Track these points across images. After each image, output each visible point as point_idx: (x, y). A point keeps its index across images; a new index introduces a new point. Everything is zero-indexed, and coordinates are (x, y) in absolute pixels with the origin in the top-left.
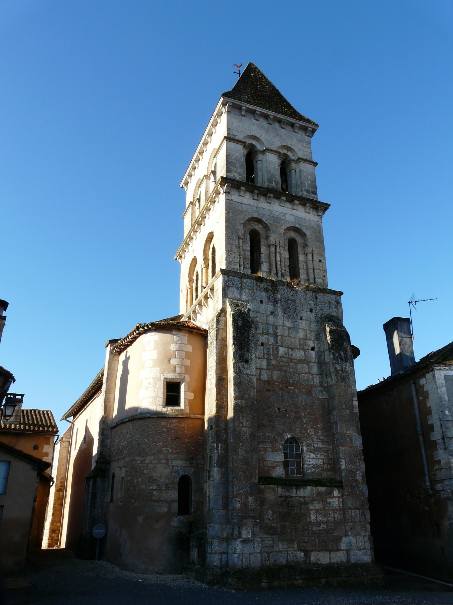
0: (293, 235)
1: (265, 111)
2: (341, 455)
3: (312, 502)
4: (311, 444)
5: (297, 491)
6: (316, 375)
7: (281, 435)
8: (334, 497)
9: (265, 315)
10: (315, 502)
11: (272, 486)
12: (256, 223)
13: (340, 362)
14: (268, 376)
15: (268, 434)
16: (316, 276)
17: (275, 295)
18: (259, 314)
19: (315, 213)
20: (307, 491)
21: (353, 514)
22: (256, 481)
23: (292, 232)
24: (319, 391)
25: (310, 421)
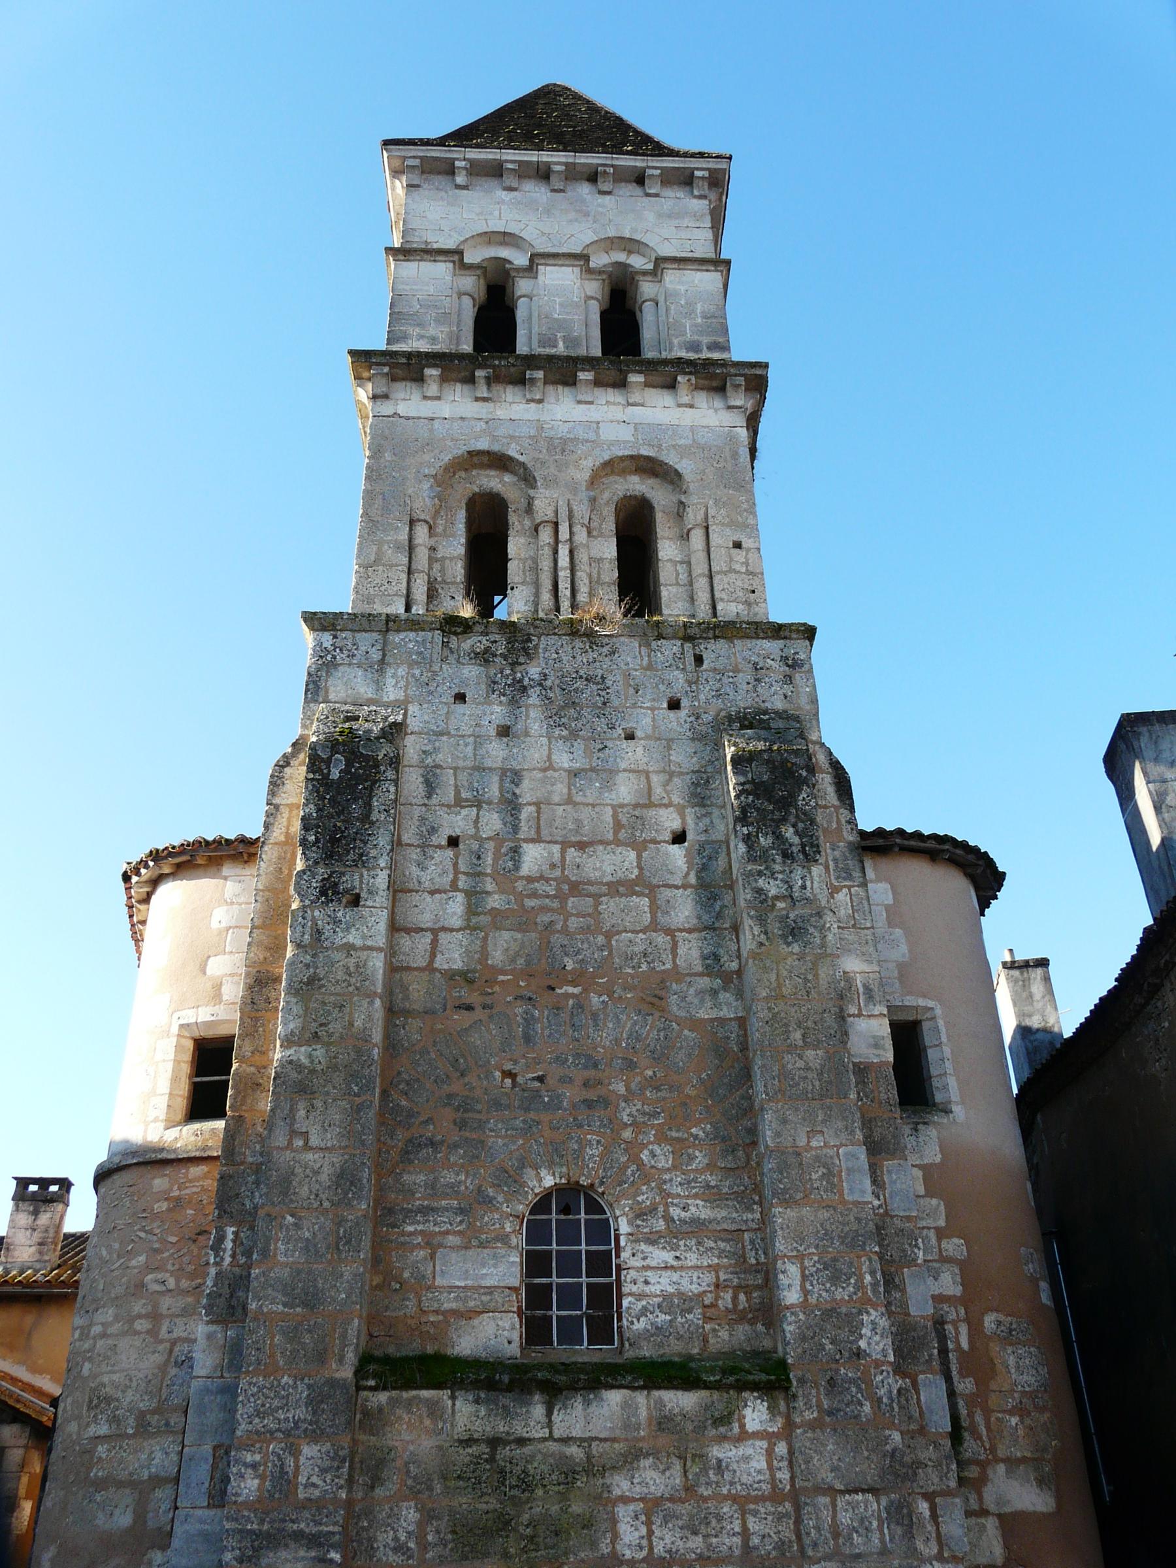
0: (636, 485)
1: (532, 156)
2: (780, 1246)
3: (630, 1459)
4: (653, 1209)
5: (549, 1413)
6: (690, 931)
7: (510, 1179)
8: (744, 1436)
9: (471, 740)
10: (646, 1463)
11: (425, 1394)
12: (493, 473)
13: (777, 867)
14: (467, 952)
15: (449, 1177)
16: (717, 595)
17: (519, 668)
18: (445, 738)
19: (718, 403)
20: (605, 1411)
21: (845, 1518)
22: (347, 1373)
23: (635, 479)
24: (699, 993)
25: (655, 1115)
